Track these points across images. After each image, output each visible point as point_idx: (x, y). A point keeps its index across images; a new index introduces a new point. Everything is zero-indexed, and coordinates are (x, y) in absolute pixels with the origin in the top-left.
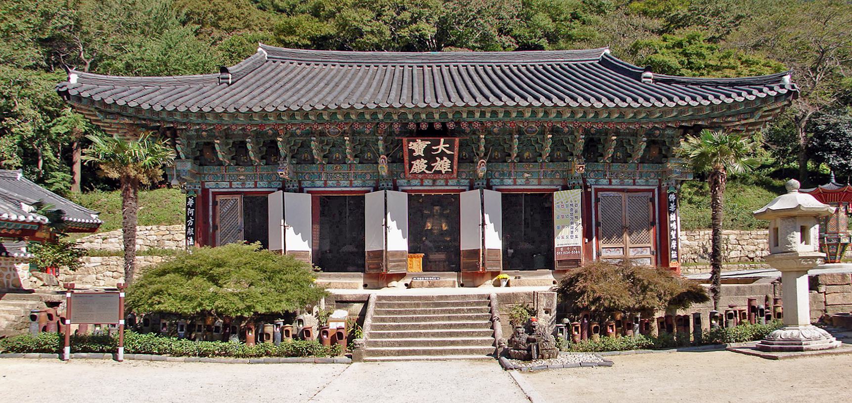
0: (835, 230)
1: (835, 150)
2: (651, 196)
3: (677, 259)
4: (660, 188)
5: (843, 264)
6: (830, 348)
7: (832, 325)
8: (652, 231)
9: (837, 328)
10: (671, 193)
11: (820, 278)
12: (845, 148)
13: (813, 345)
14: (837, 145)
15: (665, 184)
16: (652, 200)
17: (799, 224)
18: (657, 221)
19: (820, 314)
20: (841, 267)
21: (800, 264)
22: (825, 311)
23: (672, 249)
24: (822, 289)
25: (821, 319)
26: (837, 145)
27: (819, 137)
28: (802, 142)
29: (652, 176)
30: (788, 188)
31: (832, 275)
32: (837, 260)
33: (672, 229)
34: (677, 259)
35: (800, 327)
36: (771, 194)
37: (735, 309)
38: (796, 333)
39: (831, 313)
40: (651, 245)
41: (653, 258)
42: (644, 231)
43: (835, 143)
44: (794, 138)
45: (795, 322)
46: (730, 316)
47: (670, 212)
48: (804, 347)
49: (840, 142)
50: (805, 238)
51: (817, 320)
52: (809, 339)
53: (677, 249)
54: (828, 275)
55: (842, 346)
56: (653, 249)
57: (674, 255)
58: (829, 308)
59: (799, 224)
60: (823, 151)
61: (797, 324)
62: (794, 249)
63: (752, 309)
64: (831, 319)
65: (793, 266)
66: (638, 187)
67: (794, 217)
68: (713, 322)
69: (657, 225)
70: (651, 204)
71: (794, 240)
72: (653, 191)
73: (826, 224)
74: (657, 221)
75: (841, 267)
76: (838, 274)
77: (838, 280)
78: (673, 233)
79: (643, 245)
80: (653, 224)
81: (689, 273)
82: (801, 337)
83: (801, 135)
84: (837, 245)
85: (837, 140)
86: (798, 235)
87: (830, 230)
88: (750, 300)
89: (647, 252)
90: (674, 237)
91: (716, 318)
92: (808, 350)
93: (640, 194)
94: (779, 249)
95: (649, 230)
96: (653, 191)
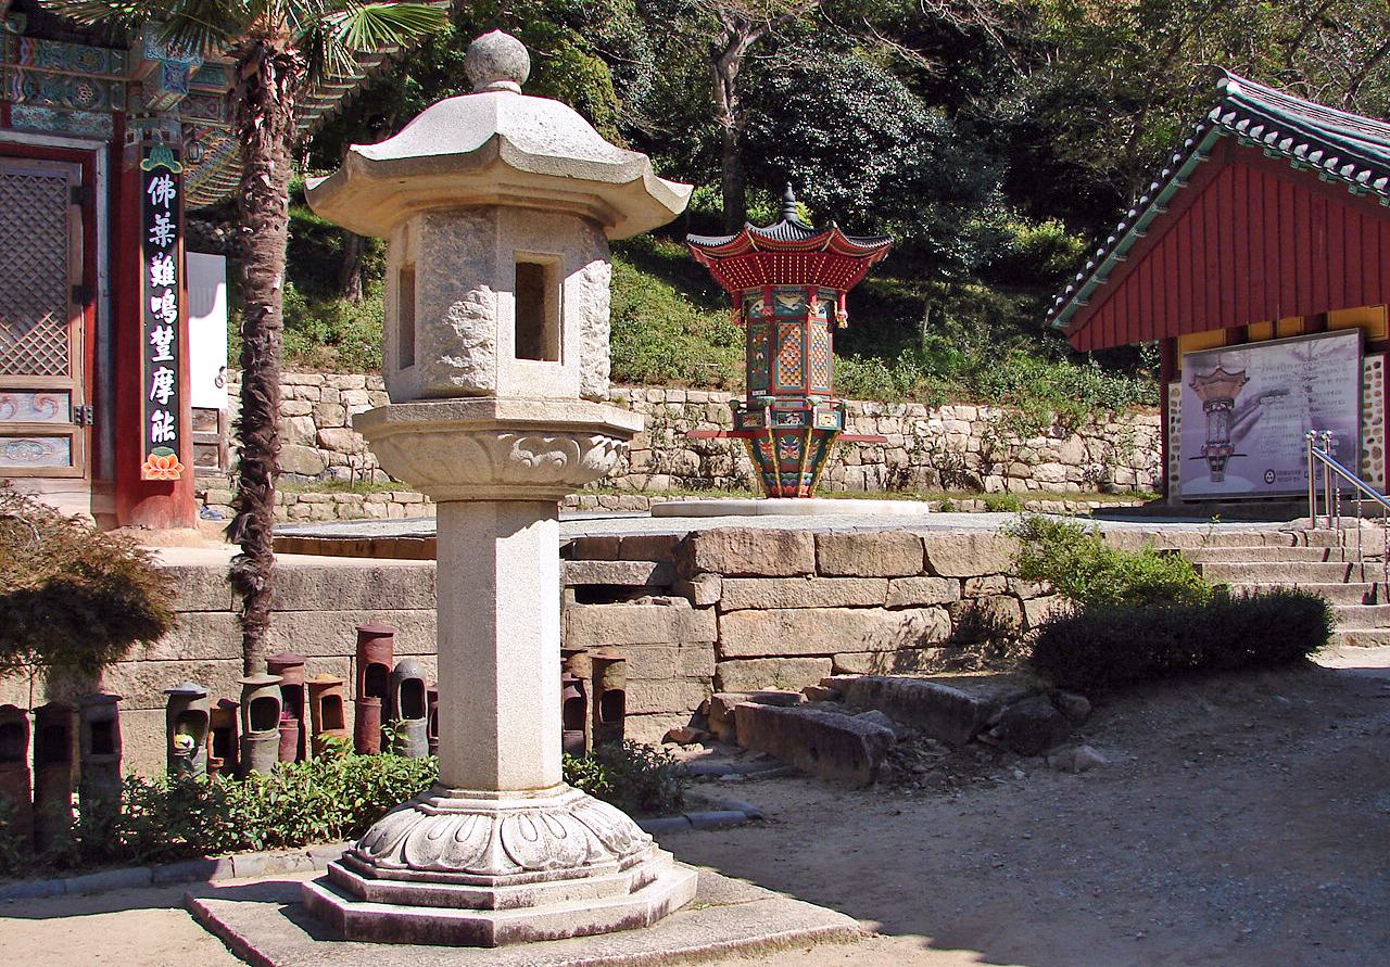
0: (796, 384)
1: (820, 153)
2: (77, 175)
3: (175, 445)
4: (116, 151)
5: (817, 501)
6: (632, 924)
7: (732, 741)
8: (78, 325)
9: (746, 762)
10: (161, 172)
11: (700, 546)
12: (844, 150)
13: (553, 906)
14: (824, 138)
15: (135, 132)
16: (83, 196)
17: (511, 249)
18: (102, 284)
19: (697, 695)
20: (809, 511)
21: (507, 463)
22: (717, 681)
23: (155, 404)
24: (708, 590)
25: (700, 716)
26: (824, 138)
27: (778, 113)
28: (729, 122)
29: (85, 95)
30: (473, 69)
31: (744, 536)
32: (803, 488)
33: (157, 321)
34: (175, 445)
35: (504, 802)
36: (645, 278)
37: (294, 677)
38: (474, 831)
39: (734, 695)
40: (76, 381)
41: (82, 437)
42: (46, 325)
43: (817, 132)
44: (710, 113)
45: (477, 774)
46: (264, 714)
47: (153, 251)
48: (499, 919)
49: (831, 129)
50: (534, 339)
51: (686, 720)
52: (532, 873)
53: (175, 406)
54: (732, 535)
55: (703, 899)
56: (80, 400)
57: (162, 429)
58: (730, 671)
59: (511, 249)
60: (789, 154)
61: (487, 782)
62: (479, 379)
63: (375, 678)
64: (732, 718)
65: (475, 471)
66: (22, 138)
67: (484, 210)
68: (184, 739)
69: (103, 302)
70: (76, 211)
71: (479, 331)
72: (87, 158)
73: (770, 361)
74: (102, 284)
75: (809, 511)
76: (766, 534)
77: (766, 559)
78: (162, 338)
79: (40, 381)
80: (83, 295)
81: (364, 517)
82: (498, 862)
83: (728, 104)
84: (801, 433)
85: (824, 126)
86: (499, 309)
87: (782, 381)
88: (366, 638)
89: (57, 413)
90: (164, 354)
91: (195, 722)
92: (517, 936)
93: (29, 166)
94: (418, 376)
95: (65, 320)
96: (87, 158)
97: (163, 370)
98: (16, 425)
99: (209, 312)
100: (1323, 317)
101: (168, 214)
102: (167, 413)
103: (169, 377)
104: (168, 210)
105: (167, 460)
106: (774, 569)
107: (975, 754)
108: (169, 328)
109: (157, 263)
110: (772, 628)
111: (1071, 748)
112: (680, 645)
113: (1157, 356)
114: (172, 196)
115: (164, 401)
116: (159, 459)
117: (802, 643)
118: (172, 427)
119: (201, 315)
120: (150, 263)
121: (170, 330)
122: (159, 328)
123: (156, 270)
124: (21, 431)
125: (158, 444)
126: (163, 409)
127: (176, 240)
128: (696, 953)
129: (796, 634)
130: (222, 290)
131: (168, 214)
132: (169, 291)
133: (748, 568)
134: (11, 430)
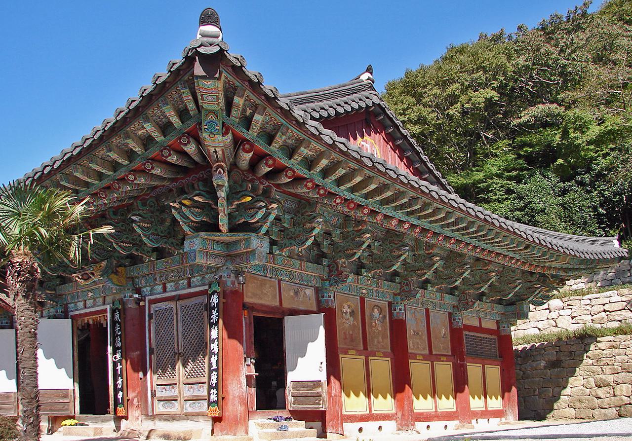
47: (211, 325)
97: (214, 373)
98: (193, 396)
99: (316, 339)
101: (216, 309)
102: (215, 390)
104: (216, 308)
105: (214, 408)
107: (477, 154)
108: (216, 355)
109: (212, 329)
113: (304, 210)
114: (217, 302)
116: (212, 408)
119: (292, 370)
120: (211, 331)
122: (213, 356)
123: (212, 333)
124: (194, 398)
125: (212, 402)
126: (214, 388)
127: (218, 319)
131: (216, 309)
132: (216, 340)
134: (191, 398)
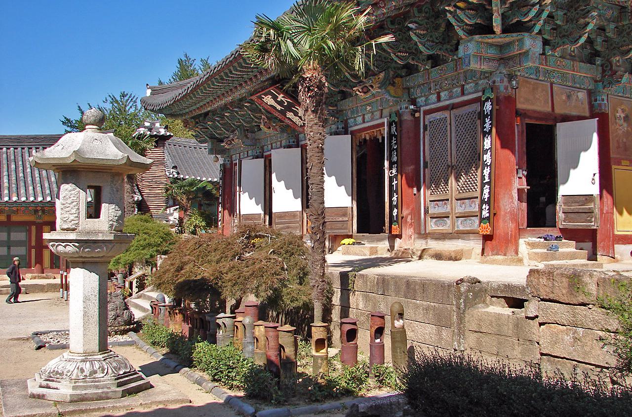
77: (561, 290)
100: (549, 45)
101: (489, 117)
103: (488, 189)
104: (489, 115)
106: (566, 298)
108: (489, 167)
109: (486, 139)
110: (568, 339)
111: (260, 404)
112: (518, 340)
114: (490, 109)
115: (486, 200)
117: (586, 353)
118: (488, 211)
121: (489, 167)
124: (466, 215)
127: (491, 128)
128: (85, 401)
129: (583, 347)
130: (595, 137)
131: (489, 117)
133: (551, 296)
